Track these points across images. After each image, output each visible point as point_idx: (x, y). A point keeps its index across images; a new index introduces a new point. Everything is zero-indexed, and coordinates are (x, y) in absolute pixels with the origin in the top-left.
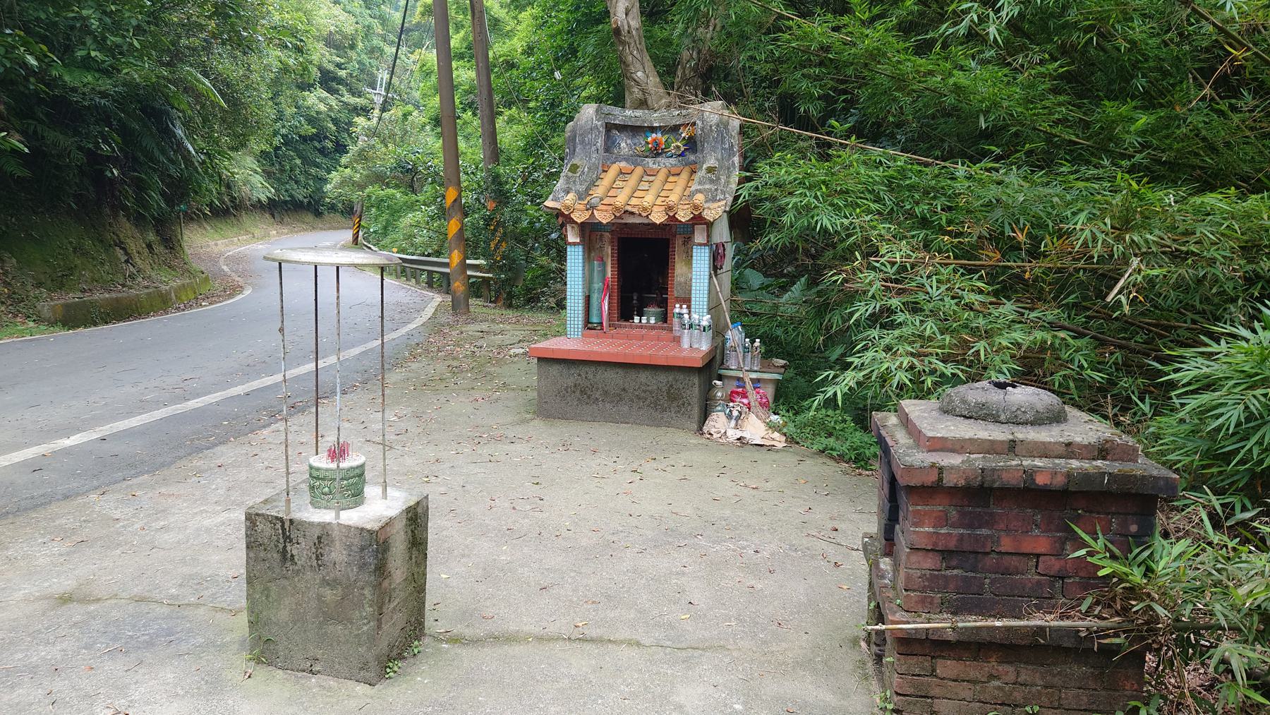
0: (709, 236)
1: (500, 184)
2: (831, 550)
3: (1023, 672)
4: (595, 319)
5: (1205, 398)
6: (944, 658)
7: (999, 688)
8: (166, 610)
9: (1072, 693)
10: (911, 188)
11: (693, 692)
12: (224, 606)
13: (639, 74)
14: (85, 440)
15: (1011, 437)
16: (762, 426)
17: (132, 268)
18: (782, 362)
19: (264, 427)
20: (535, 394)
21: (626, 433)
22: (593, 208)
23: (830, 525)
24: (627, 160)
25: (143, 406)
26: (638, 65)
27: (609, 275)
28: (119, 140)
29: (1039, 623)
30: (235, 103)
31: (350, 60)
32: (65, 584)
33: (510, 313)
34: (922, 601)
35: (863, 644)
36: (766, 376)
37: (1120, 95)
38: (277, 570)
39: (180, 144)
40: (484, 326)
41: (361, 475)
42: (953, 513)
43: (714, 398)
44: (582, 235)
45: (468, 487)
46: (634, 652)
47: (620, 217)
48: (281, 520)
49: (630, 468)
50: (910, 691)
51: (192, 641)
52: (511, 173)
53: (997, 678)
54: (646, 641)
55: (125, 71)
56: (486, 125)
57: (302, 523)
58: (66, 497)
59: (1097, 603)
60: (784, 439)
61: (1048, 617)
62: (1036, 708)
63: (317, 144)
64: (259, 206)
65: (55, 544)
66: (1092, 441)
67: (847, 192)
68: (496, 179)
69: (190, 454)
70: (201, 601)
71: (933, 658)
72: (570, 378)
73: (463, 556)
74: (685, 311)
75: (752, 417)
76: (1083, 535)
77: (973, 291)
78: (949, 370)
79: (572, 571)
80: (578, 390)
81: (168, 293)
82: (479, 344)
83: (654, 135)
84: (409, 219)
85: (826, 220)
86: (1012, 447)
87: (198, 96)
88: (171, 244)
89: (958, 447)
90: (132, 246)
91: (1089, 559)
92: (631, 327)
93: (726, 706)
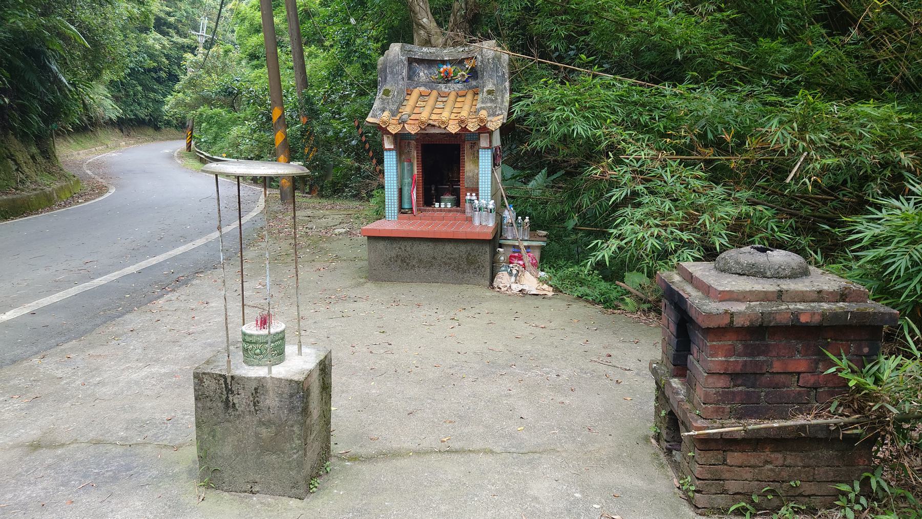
0: (491, 142)
1: (312, 104)
2: (610, 371)
3: (789, 457)
4: (406, 206)
5: (882, 251)
6: (732, 451)
7: (771, 470)
8: (120, 450)
9: (822, 470)
10: (635, 103)
11: (545, 486)
12: (166, 443)
13: (425, 20)
14: (19, 314)
15: (778, 288)
16: (535, 281)
17: (21, 175)
18: (545, 233)
19: (159, 297)
20: (366, 263)
21: (438, 290)
22: (404, 122)
23: (605, 352)
24: (425, 85)
25: (58, 286)
26: (424, 14)
27: (416, 172)
28: (8, 75)
29: (803, 422)
30: (96, 44)
31: (180, 9)
32: (32, 433)
33: (324, 202)
34: (717, 411)
35: (653, 441)
36: (534, 244)
37: (773, 35)
38: (222, 416)
39: (56, 77)
40: (309, 212)
41: (283, 338)
42: (739, 346)
43: (498, 261)
44: (395, 143)
45: (331, 337)
46: (490, 458)
47: (424, 129)
48: (224, 377)
49: (448, 317)
50: (709, 476)
51: (149, 474)
52: (317, 94)
53: (770, 463)
54: (497, 449)
55: (11, 21)
56: (297, 60)
57: (242, 378)
58: (14, 362)
59: (840, 405)
60: (551, 289)
61: (810, 417)
62: (798, 483)
63: (153, 75)
64: (111, 123)
65: (14, 401)
66: (836, 288)
67: (593, 107)
68: (309, 101)
69: (105, 322)
70: (147, 441)
71: (724, 451)
72: (394, 250)
73: (343, 392)
74: (474, 198)
75: (527, 274)
76: (832, 357)
77: (696, 178)
78: (685, 236)
79: (428, 398)
80: (400, 260)
81: (51, 193)
82: (309, 226)
83: (445, 67)
84: (235, 131)
85: (580, 128)
86: (780, 295)
87: (66, 38)
88: (48, 154)
89: (741, 297)
90: (21, 157)
91: (839, 374)
92: (433, 211)
93: (569, 495)
